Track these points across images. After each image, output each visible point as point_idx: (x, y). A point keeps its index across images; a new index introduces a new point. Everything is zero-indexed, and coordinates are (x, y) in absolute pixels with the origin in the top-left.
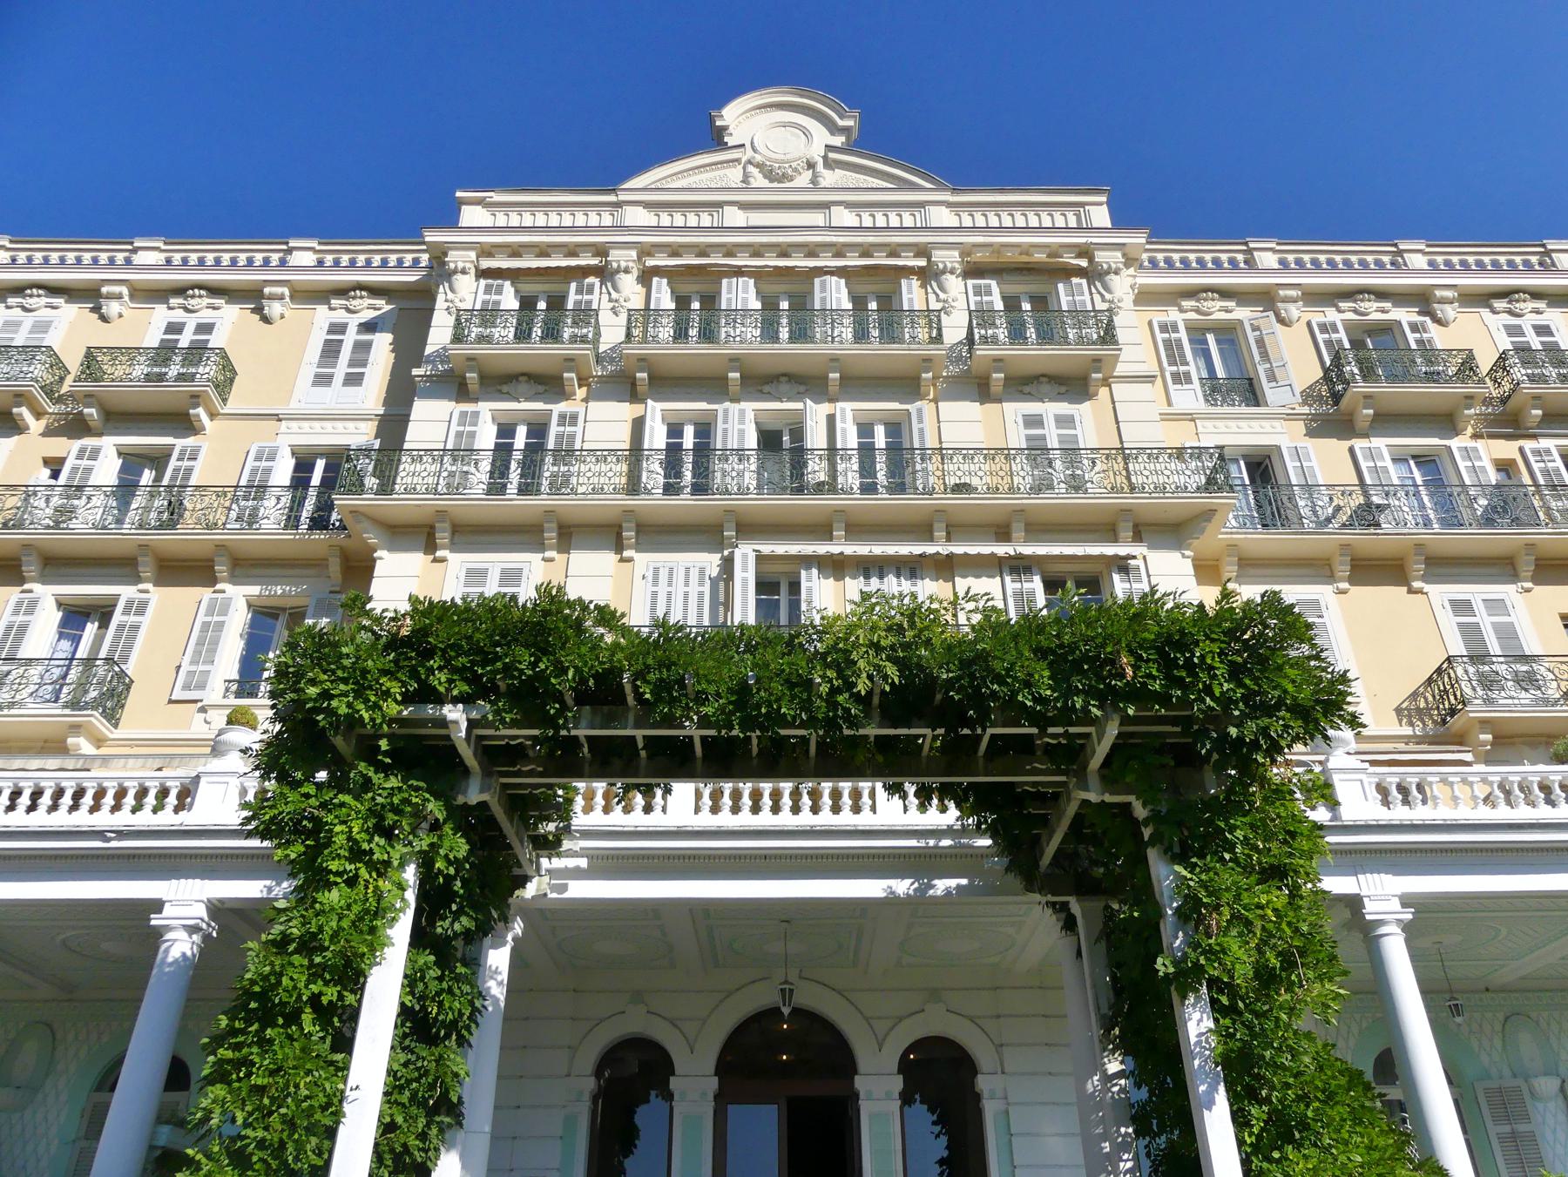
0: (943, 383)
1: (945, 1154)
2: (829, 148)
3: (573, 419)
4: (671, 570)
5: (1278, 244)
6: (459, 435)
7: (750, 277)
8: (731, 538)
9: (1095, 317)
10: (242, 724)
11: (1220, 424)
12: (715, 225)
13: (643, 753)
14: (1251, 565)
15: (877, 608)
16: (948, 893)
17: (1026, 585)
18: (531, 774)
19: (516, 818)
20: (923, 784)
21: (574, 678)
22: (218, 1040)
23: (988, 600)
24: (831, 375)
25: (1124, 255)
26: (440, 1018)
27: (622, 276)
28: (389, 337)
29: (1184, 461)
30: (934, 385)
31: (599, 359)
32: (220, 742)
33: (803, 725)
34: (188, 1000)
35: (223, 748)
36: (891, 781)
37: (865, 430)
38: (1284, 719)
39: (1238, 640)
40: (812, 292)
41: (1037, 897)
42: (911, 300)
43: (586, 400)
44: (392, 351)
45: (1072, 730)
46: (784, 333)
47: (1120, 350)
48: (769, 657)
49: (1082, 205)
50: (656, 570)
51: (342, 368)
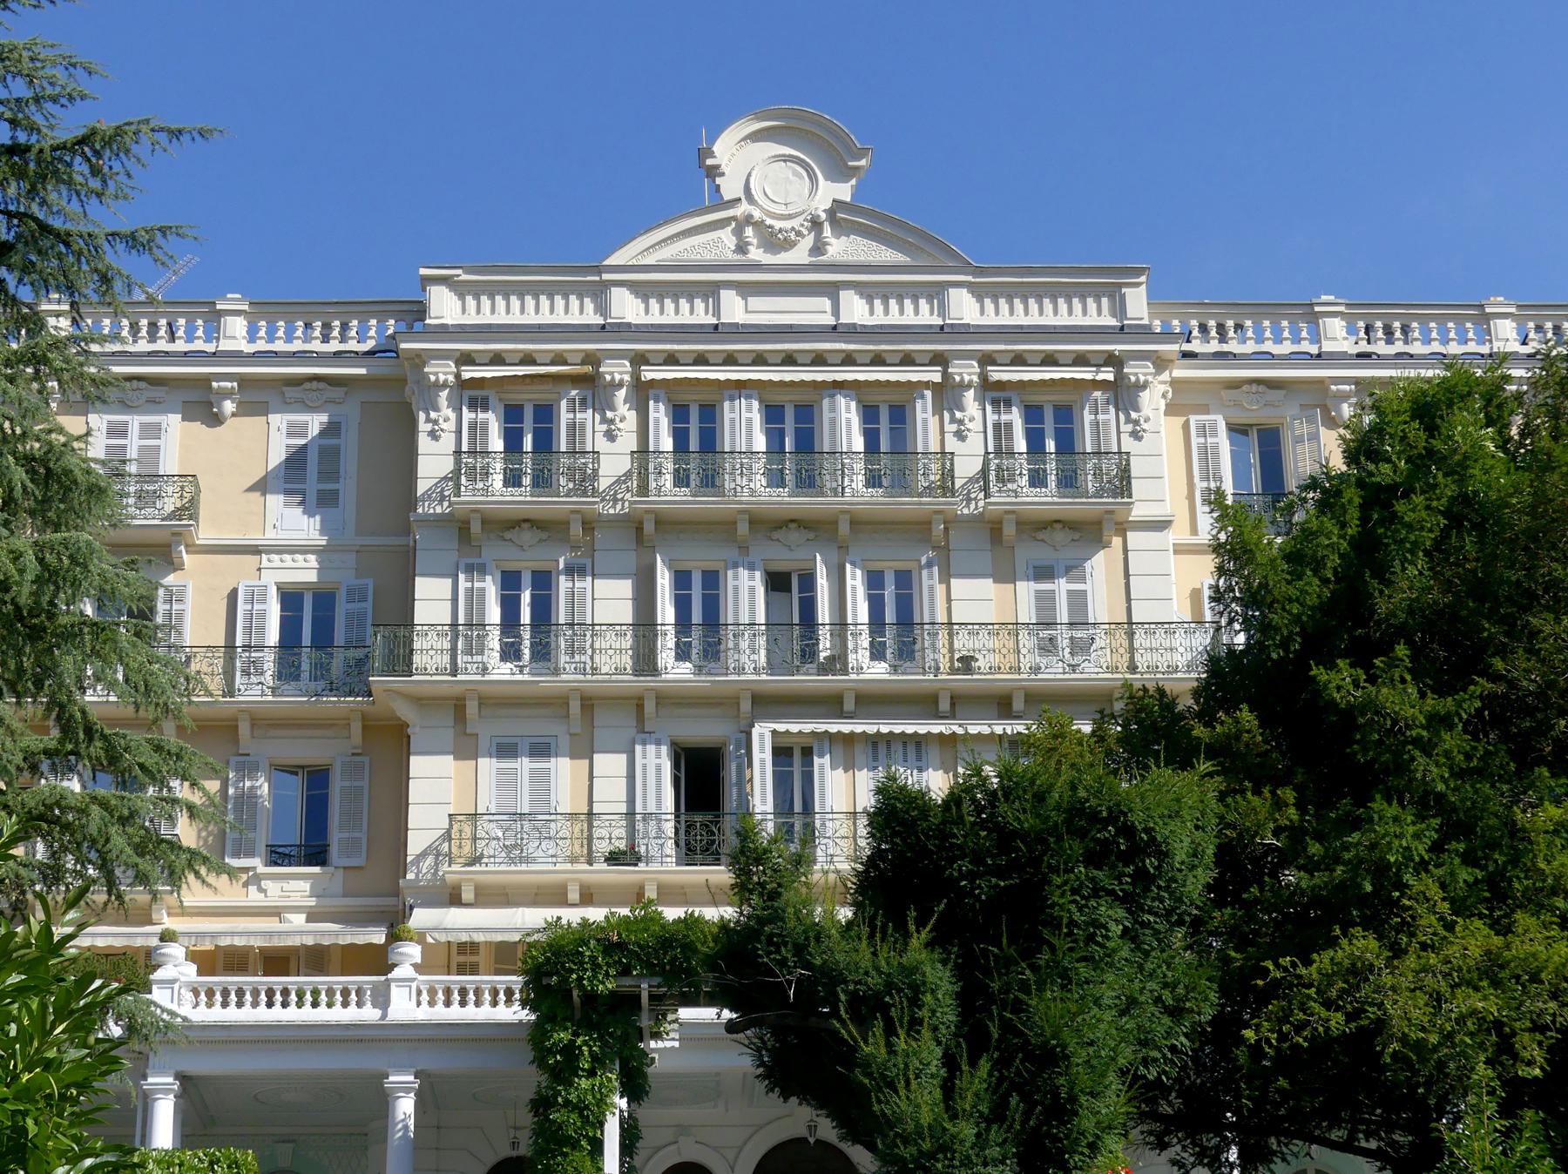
49: (1121, 285)
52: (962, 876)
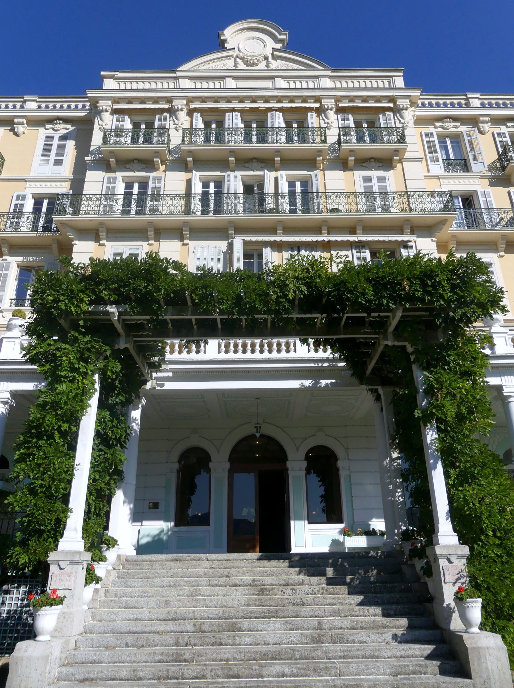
0: (327, 162)
1: (323, 493)
2: (274, 49)
3: (159, 180)
4: (205, 249)
5: (481, 95)
6: (108, 188)
7: (239, 112)
8: (232, 234)
9: (396, 130)
10: (19, 317)
11: (451, 181)
12: (222, 87)
13: (195, 327)
14: (461, 244)
15: (297, 262)
16: (327, 385)
17: (363, 254)
18: (147, 336)
19: (141, 356)
20: (317, 339)
21: (164, 294)
22: (19, 446)
23: (346, 258)
24: (276, 159)
25: (410, 101)
26: (113, 437)
27: (179, 112)
28: (73, 142)
29: (434, 197)
30: (323, 163)
31: (170, 152)
32: (10, 324)
33: (265, 313)
34: (5, 433)
35: (12, 327)
36: (303, 337)
37: (292, 184)
38: (473, 309)
39: (455, 274)
40: (267, 120)
41: (365, 387)
42: (312, 123)
43: (165, 171)
44: (75, 149)
45: (382, 314)
46: (254, 139)
47: (407, 146)
48: (250, 283)
49: (391, 77)
50: (199, 249)
51: (52, 157)
52: (398, 138)
